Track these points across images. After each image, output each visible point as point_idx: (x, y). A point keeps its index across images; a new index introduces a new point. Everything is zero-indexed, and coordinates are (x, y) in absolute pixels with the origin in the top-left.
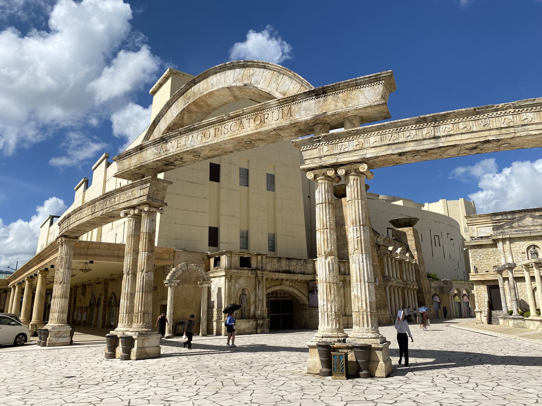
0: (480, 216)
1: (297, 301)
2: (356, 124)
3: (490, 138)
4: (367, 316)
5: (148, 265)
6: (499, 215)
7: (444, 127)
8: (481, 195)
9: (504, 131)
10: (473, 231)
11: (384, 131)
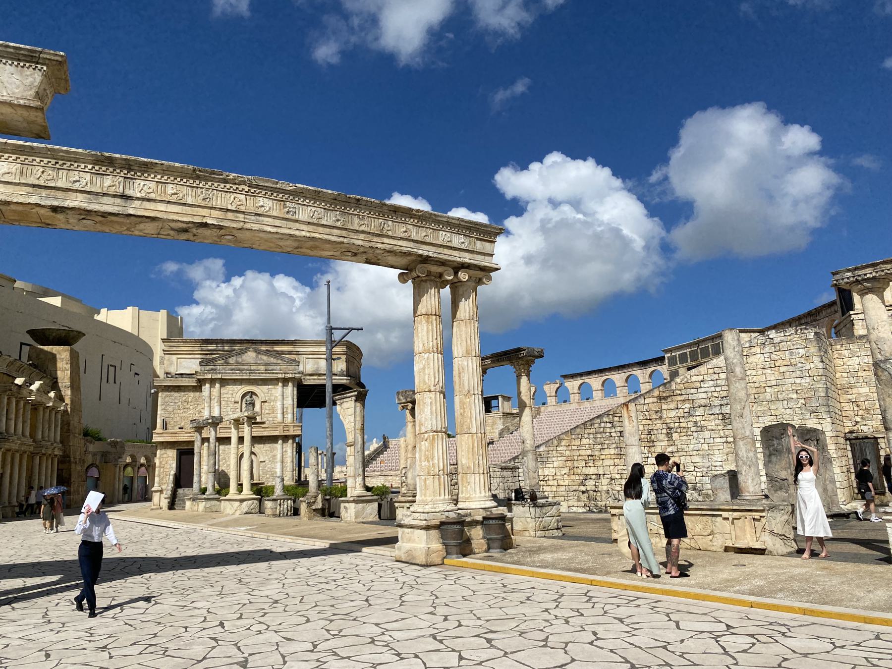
0: (185, 342)
3: (210, 221)
6: (213, 342)
7: (142, 183)
8: (196, 310)
9: (230, 215)
10: (171, 364)
11: (30, 158)
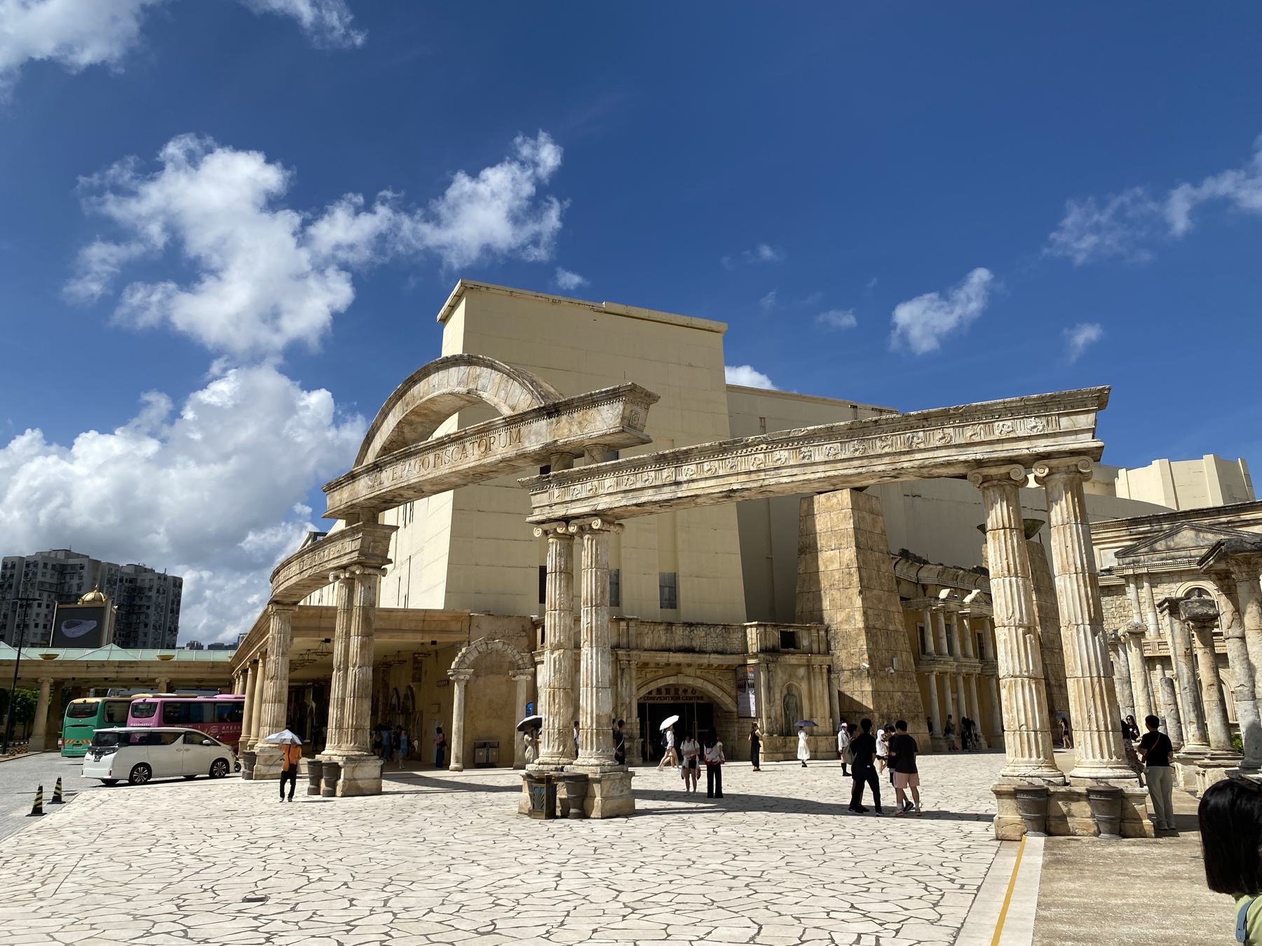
1: (719, 707)
2: (597, 457)
3: (735, 488)
4: (592, 735)
5: (362, 657)
9: (753, 477)
